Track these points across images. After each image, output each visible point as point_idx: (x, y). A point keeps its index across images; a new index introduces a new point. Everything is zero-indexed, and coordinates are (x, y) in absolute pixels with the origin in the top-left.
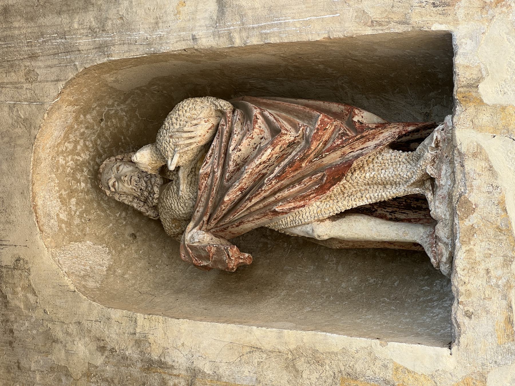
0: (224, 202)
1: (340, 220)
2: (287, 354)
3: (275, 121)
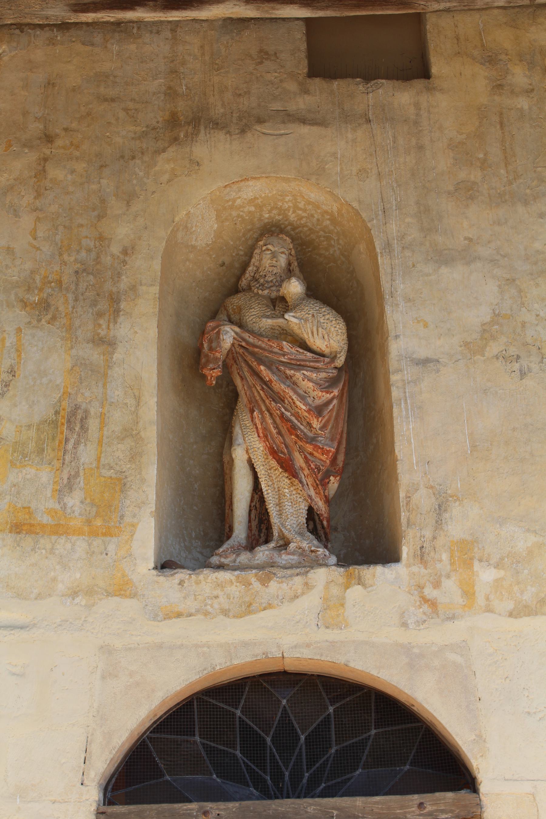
0: (259, 364)
1: (248, 467)
2: (136, 430)
3: (328, 410)
